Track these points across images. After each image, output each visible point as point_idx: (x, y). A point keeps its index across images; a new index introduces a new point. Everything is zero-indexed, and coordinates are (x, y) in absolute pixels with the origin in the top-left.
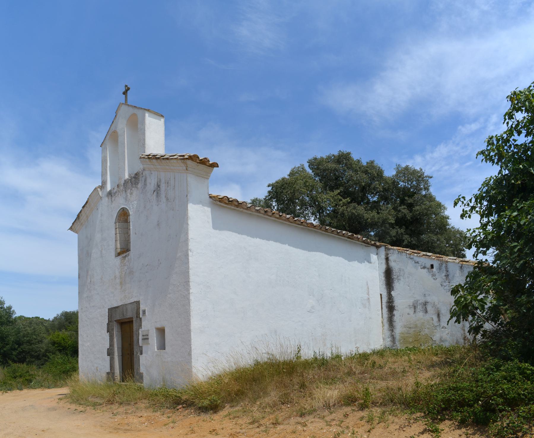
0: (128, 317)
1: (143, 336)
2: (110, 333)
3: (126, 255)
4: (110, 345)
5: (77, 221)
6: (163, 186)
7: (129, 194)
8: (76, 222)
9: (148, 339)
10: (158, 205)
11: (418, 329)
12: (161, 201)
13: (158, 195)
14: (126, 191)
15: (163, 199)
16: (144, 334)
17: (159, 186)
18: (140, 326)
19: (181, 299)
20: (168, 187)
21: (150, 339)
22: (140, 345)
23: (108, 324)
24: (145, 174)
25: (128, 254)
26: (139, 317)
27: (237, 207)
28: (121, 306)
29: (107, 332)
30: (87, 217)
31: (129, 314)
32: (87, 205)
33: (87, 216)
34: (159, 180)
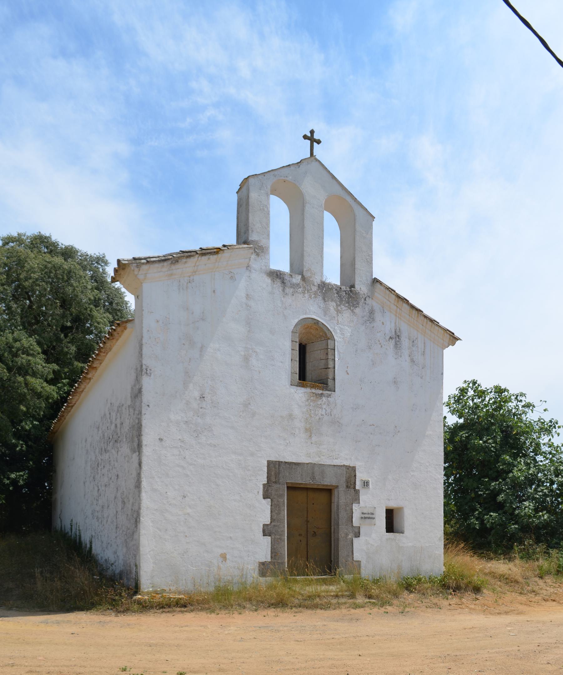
2: (272, 500)
5: (165, 264)
8: (162, 264)
13: (397, 346)
16: (365, 512)
19: (431, 481)
21: (376, 519)
22: (354, 525)
26: (355, 488)
28: (307, 464)
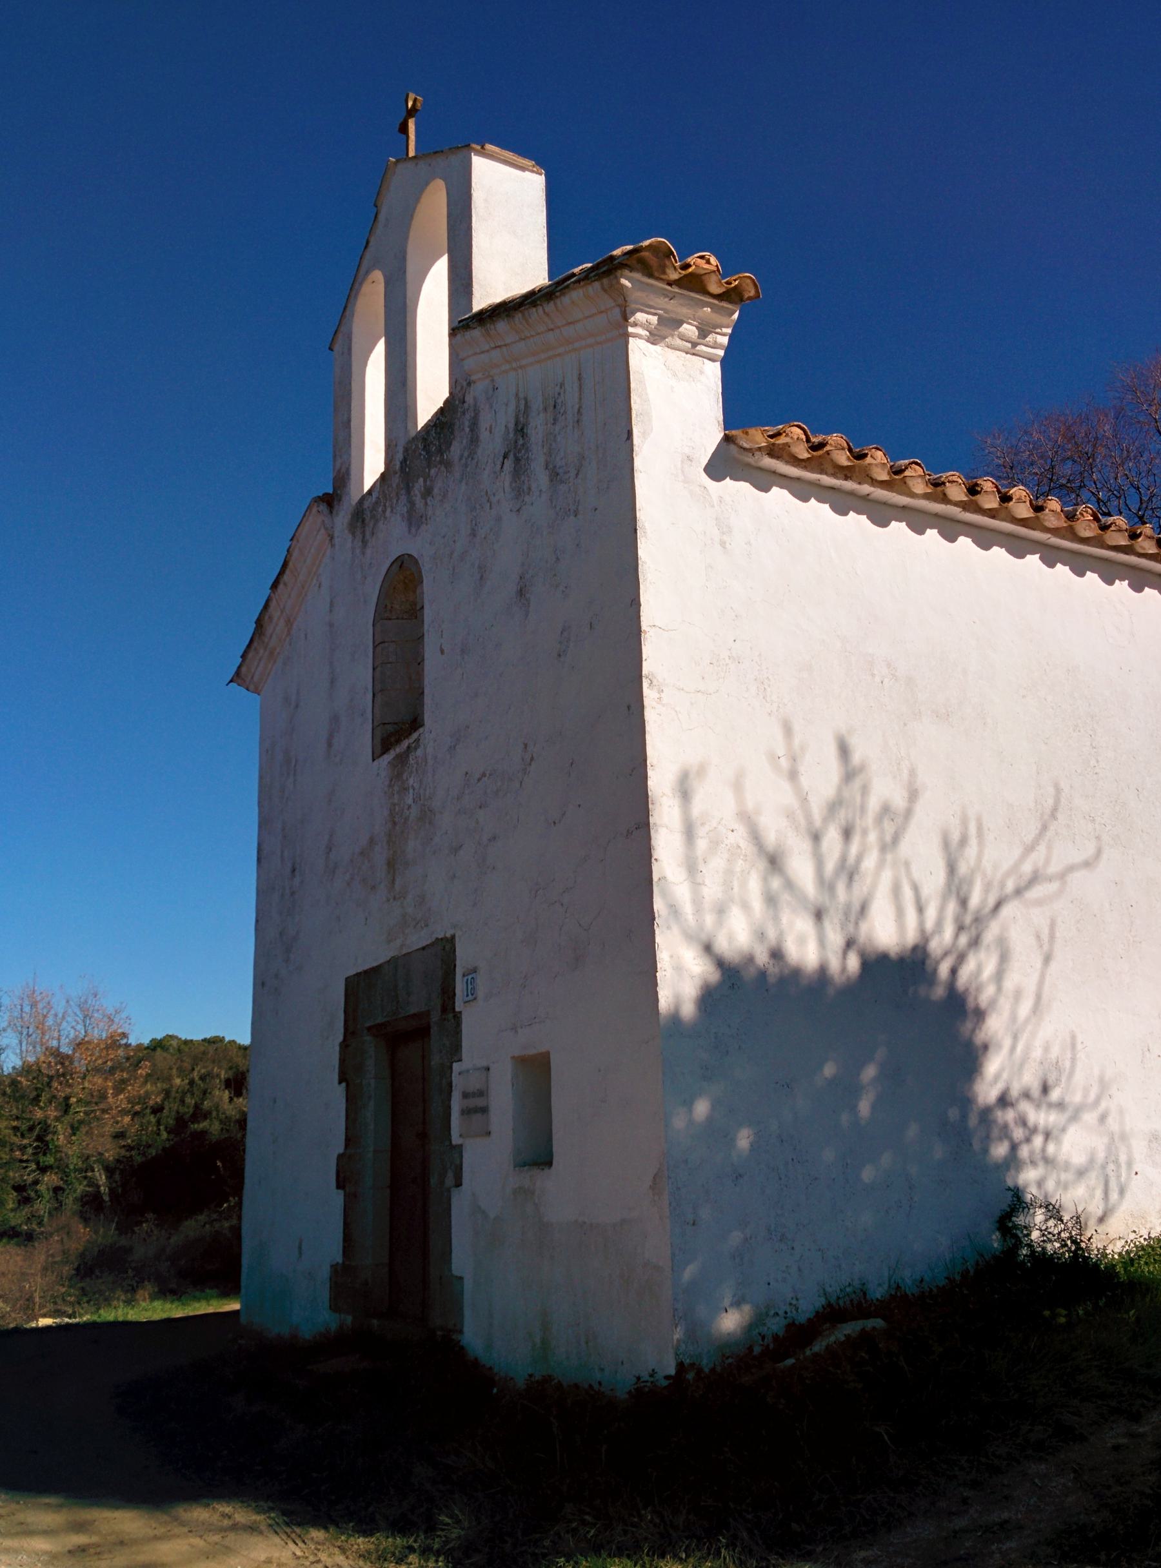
0: (412, 1012)
1: (465, 1095)
2: (347, 1086)
3: (409, 747)
4: (348, 1141)
5: (255, 644)
6: (538, 426)
7: (418, 500)
9: (484, 1110)
10: (518, 510)
11: (129, 1141)
12: (529, 489)
14: (408, 490)
15: (540, 477)
17: (522, 429)
18: (455, 1050)
20: (555, 421)
22: (454, 1143)
23: (344, 1045)
24: (475, 399)
25: (417, 740)
27: (846, 478)
29: (340, 1082)
30: (289, 623)
31: (419, 1000)
32: (286, 577)
33: (289, 621)
34: (522, 407)
